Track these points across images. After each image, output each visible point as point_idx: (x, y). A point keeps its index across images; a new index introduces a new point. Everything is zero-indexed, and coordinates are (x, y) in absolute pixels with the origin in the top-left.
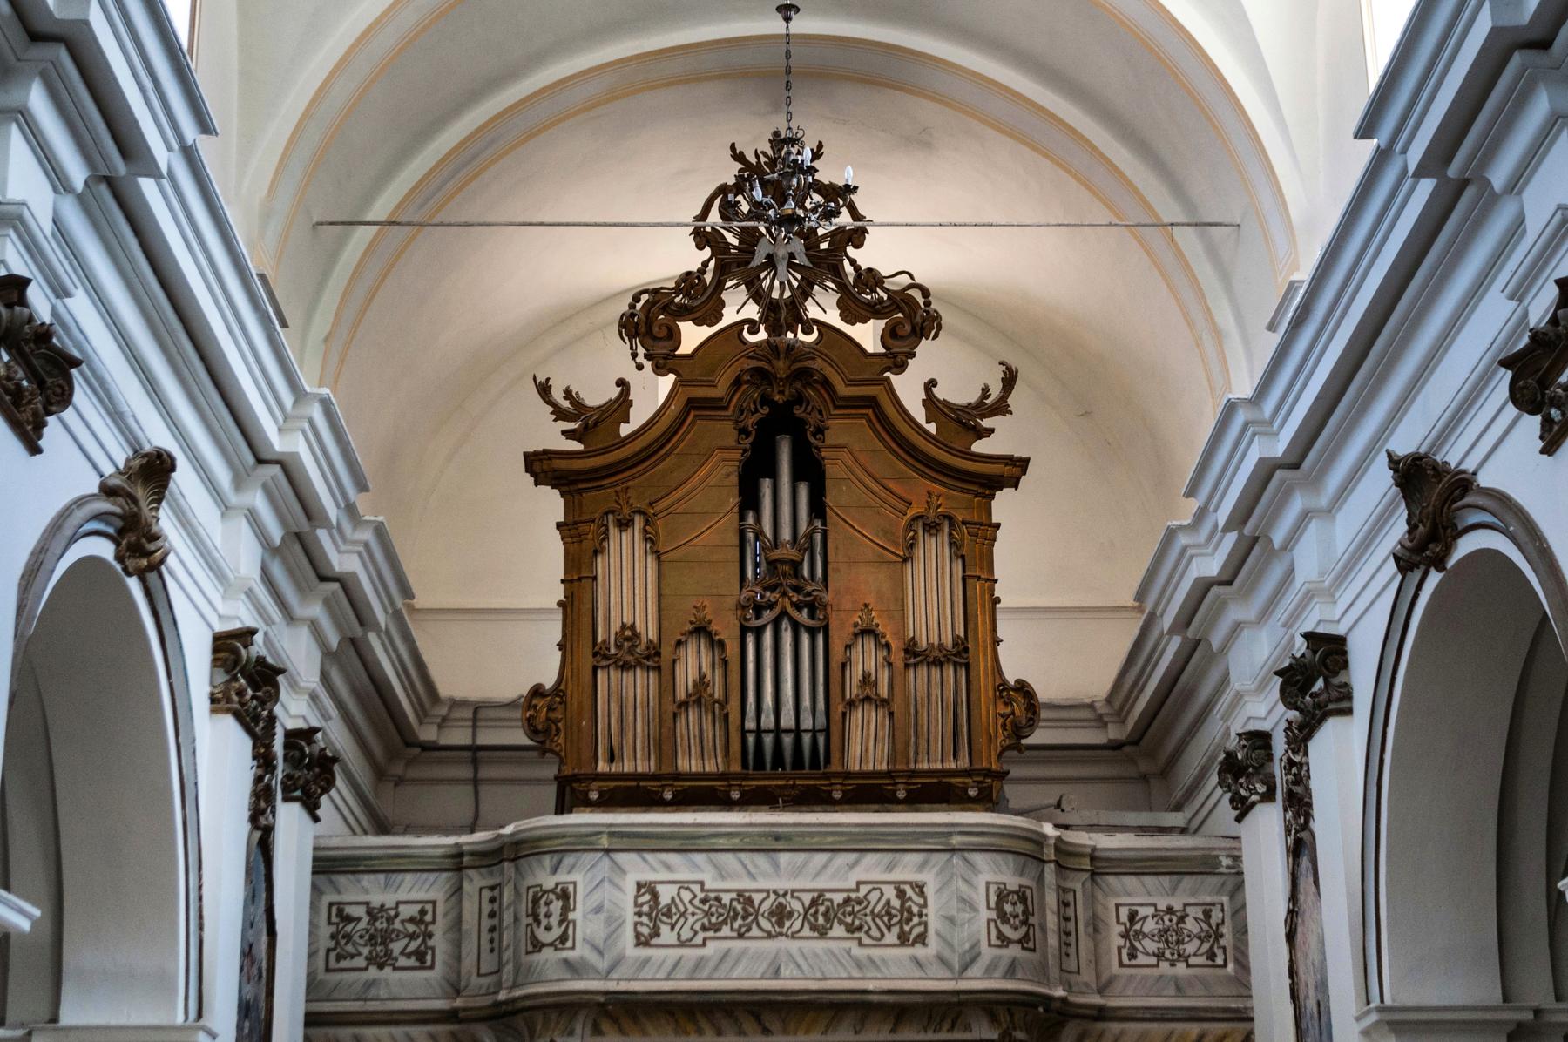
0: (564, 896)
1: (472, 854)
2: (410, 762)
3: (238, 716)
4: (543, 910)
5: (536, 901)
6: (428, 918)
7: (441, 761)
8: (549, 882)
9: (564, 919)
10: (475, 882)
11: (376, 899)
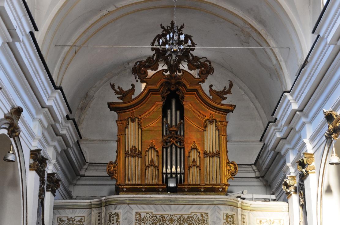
0: (117, 215)
1: (94, 204)
2: (79, 179)
3: (37, 171)
4: (112, 219)
5: (110, 217)
6: (83, 221)
7: (86, 180)
8: (113, 212)
9: (117, 221)
10: (95, 211)
11: (69, 216)
